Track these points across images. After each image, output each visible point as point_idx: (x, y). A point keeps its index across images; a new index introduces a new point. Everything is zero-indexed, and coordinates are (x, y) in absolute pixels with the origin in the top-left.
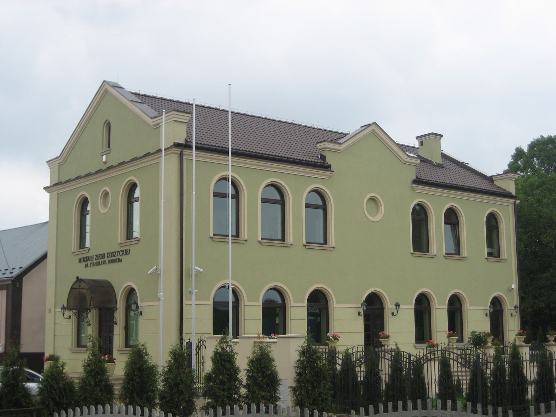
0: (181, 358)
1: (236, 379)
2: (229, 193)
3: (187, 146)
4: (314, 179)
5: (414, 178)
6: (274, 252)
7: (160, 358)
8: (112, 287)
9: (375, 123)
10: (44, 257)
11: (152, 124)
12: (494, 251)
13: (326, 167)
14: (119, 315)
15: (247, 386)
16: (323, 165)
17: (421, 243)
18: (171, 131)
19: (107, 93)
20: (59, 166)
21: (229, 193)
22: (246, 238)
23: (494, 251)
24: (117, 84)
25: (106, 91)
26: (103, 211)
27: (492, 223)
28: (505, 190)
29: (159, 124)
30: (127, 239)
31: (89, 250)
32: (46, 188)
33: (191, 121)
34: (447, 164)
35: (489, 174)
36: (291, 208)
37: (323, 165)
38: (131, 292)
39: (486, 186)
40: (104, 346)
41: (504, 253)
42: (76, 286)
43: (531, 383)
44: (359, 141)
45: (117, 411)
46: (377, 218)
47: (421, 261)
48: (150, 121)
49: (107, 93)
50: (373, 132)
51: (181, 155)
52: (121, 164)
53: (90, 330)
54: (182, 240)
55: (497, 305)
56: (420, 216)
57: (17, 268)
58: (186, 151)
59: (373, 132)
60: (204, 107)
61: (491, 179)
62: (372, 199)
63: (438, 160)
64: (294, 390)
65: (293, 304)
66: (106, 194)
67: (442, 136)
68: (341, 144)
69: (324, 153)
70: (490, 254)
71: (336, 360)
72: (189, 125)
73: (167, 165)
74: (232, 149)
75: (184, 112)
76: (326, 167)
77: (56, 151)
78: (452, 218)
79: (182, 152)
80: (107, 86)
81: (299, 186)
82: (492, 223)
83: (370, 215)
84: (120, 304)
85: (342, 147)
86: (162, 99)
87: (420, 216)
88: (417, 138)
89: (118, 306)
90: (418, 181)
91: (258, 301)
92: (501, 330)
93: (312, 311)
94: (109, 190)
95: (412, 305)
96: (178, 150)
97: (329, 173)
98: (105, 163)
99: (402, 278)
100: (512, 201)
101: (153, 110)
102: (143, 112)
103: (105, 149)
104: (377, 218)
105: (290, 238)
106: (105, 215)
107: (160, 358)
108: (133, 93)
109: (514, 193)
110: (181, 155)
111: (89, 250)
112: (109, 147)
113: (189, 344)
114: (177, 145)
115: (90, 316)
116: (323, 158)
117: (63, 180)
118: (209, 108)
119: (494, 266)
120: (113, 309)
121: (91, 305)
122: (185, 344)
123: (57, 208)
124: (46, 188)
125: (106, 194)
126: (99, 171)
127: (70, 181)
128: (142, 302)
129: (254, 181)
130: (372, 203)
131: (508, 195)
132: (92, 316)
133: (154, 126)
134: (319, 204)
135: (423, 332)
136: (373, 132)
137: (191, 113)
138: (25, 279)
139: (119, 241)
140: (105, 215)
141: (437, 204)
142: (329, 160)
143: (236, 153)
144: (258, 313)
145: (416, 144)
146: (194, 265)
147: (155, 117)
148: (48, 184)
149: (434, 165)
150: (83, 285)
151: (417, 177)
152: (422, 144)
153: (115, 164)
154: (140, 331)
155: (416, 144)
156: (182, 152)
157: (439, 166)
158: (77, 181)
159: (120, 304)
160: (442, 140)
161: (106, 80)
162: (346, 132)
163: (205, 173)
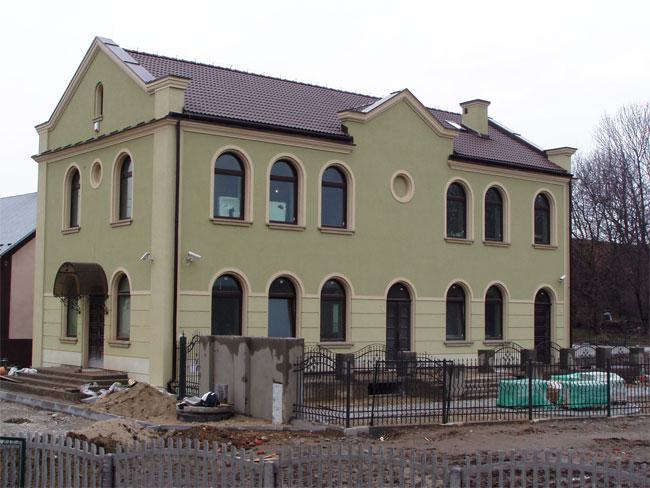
2: (232, 173)
4: (333, 155)
5: (452, 153)
6: (285, 237)
9: (407, 90)
10: (32, 236)
11: (146, 90)
12: (543, 234)
14: (111, 304)
16: (344, 139)
17: (457, 224)
18: (169, 101)
21: (232, 173)
22: (251, 220)
25: (99, 49)
26: (95, 185)
29: (153, 90)
30: (121, 218)
32: (34, 157)
34: (495, 135)
35: (543, 147)
37: (344, 139)
38: (122, 279)
39: (538, 162)
42: (64, 270)
45: (199, 446)
46: (406, 198)
48: (145, 86)
49: (98, 51)
51: (178, 127)
52: (113, 134)
53: (81, 322)
55: (544, 300)
56: (457, 196)
57: (6, 245)
59: (404, 100)
60: (212, 67)
61: (544, 154)
62: (401, 177)
63: (484, 130)
65: (354, 296)
66: (98, 167)
67: (489, 103)
68: (365, 113)
69: (346, 124)
73: (164, 138)
75: (180, 77)
77: (45, 116)
78: (495, 200)
79: (178, 123)
83: (397, 193)
84: (112, 291)
85: (366, 118)
86: (164, 58)
87: (457, 196)
88: (461, 104)
89: (109, 293)
91: (264, 291)
93: (452, 299)
94: (98, 160)
97: (349, 147)
98: (97, 131)
99: (435, 267)
101: (150, 75)
102: (143, 74)
103: (98, 115)
104: (406, 198)
105: (303, 221)
106: (98, 189)
108: (126, 50)
110: (178, 127)
113: (183, 339)
114: (173, 115)
115: (79, 302)
116: (344, 129)
117: (53, 149)
118: (219, 68)
119: (543, 255)
120: (104, 296)
122: (178, 339)
123: (46, 180)
124: (34, 157)
125: (98, 167)
126: (91, 141)
127: (63, 152)
128: (181, 289)
129: (261, 158)
130: (401, 183)
132: (81, 304)
134: (337, 183)
135: (456, 326)
136: (404, 100)
138: (14, 256)
139: (111, 222)
140: (98, 189)
142: (351, 132)
144: (206, 304)
145: (460, 111)
146: (190, 250)
147: (149, 83)
148: (36, 152)
150: (71, 270)
151: (454, 152)
152: (466, 111)
153: (107, 134)
154: (132, 322)
155: (460, 111)
156: (178, 123)
157: (485, 138)
158: (67, 151)
159: (112, 291)
160: (489, 107)
162: (378, 96)
163: (208, 148)
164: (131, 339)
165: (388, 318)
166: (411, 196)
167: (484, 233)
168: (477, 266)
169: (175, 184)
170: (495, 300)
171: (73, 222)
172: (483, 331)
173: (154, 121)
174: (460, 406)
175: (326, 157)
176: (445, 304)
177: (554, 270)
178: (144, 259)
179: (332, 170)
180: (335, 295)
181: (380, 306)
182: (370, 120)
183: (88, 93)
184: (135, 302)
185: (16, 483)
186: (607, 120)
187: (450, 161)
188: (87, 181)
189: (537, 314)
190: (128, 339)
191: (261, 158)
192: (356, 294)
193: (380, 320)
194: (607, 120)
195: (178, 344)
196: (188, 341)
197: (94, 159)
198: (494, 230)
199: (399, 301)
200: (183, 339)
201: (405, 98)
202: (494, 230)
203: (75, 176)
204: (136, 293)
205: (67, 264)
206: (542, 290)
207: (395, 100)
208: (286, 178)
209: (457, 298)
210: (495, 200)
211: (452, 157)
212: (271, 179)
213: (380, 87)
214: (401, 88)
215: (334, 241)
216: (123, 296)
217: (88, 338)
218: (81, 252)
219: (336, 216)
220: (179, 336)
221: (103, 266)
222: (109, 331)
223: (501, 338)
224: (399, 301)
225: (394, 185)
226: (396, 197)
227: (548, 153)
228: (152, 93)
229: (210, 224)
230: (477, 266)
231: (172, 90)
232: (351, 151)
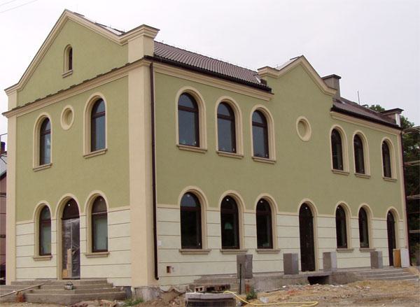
2: (190, 106)
12: (387, 172)
13: (268, 90)
19: (67, 21)
20: (18, 92)
21: (190, 106)
23: (387, 172)
26: (66, 127)
27: (386, 147)
29: (126, 41)
31: (51, 165)
32: (3, 114)
36: (241, 124)
41: (394, 175)
44: (291, 70)
46: (307, 138)
50: (300, 65)
51: (151, 67)
54: (153, 146)
56: (337, 137)
59: (301, 64)
62: (302, 122)
65: (278, 213)
67: (340, 78)
73: (138, 81)
77: (15, 79)
79: (151, 65)
80: (68, 14)
82: (386, 147)
87: (337, 137)
92: (200, 277)
94: (71, 108)
95: (333, 214)
100: (400, 132)
103: (66, 71)
104: (307, 138)
109: (400, 126)
111: (51, 165)
112: (70, 67)
114: (147, 58)
124: (3, 114)
125: (69, 112)
128: (158, 203)
131: (396, 127)
133: (121, 43)
134: (261, 121)
136: (301, 64)
140: (70, 130)
156: (151, 65)
158: (38, 104)
161: (67, 8)
163: (175, 85)
166: (310, 132)
167: (355, 169)
169: (150, 102)
171: (42, 159)
173: (128, 65)
175: (257, 101)
181: (295, 221)
182: (283, 76)
183: (60, 57)
184: (112, 217)
185: (334, 106)
187: (332, 112)
188: (59, 126)
191: (210, 99)
192: (279, 211)
193: (296, 232)
197: (66, 105)
199: (306, 217)
201: (301, 62)
207: (294, 64)
208: (228, 113)
212: (218, 117)
213: (279, 59)
214: (300, 55)
217: (61, 261)
222: (84, 246)
225: (299, 127)
226: (301, 137)
228: (125, 43)
231: (146, 39)
232: (271, 99)
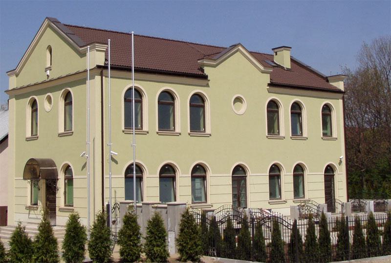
0: (103, 222)
1: (138, 233)
2: (133, 98)
3: (105, 67)
7: (87, 222)
8: (53, 162)
14: (61, 184)
15: (146, 238)
21: (133, 98)
24: (56, 19)
28: (336, 87)
33: (107, 50)
35: (326, 73)
38: (67, 169)
39: (321, 84)
40: (51, 210)
43: (351, 228)
47: (274, 142)
55: (330, 171)
56: (273, 107)
58: (104, 71)
61: (327, 79)
64: (177, 240)
70: (325, 134)
71: (206, 220)
72: (106, 52)
74: (135, 67)
76: (205, 77)
78: (296, 109)
81: (183, 93)
84: (61, 177)
87: (273, 107)
90: (271, 85)
96: (99, 71)
100: (341, 95)
107: (87, 222)
108: (65, 25)
113: (108, 206)
114: (99, 67)
118: (122, 33)
121: (39, 176)
134: (197, 103)
135: (274, 192)
137: (108, 44)
141: (286, 101)
143: (137, 70)
149: (285, 70)
159: (61, 177)
164: (74, 206)
165: (233, 187)
168: (286, 152)
170: (299, 171)
172: (292, 193)
174: (303, 223)
176: (268, 177)
177: (336, 152)
178: (82, 156)
179: (197, 96)
180: (199, 172)
181: (227, 181)
186: (365, 46)
189: (326, 181)
190: (73, 206)
194: (365, 46)
195: (105, 209)
196: (112, 205)
198: (297, 128)
199: (239, 175)
200: (108, 206)
202: (297, 128)
203: (34, 104)
204: (77, 177)
205: (32, 160)
206: (328, 166)
209: (275, 172)
210: (296, 109)
211: (269, 85)
215: (197, 141)
216: (69, 181)
218: (39, 152)
219: (197, 123)
220: (106, 203)
221: (53, 159)
223: (304, 197)
224: (239, 175)
227: (329, 79)
229: (267, 139)
230: (286, 152)
